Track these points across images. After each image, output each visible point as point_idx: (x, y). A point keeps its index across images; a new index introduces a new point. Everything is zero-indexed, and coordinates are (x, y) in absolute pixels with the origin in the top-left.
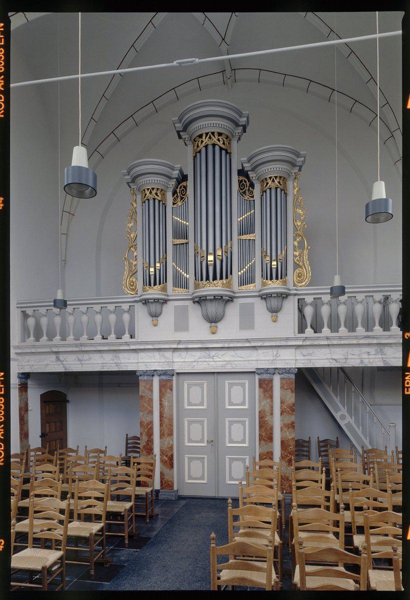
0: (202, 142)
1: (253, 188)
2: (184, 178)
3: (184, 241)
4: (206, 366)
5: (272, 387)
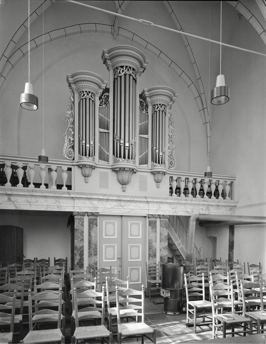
1: (148, 107)
2: (107, 90)
3: (106, 131)
4: (118, 211)
5: (156, 226)
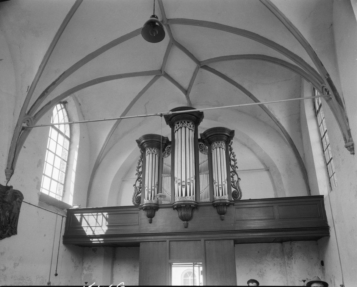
0: (179, 126)
